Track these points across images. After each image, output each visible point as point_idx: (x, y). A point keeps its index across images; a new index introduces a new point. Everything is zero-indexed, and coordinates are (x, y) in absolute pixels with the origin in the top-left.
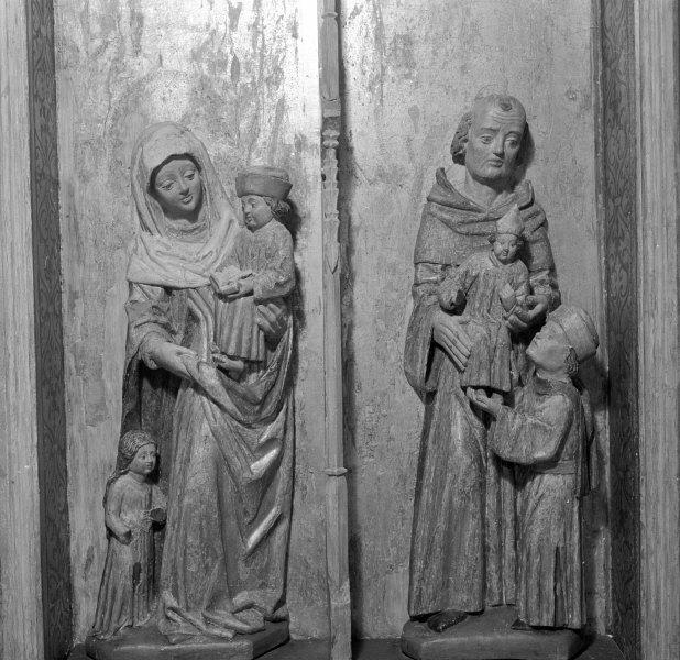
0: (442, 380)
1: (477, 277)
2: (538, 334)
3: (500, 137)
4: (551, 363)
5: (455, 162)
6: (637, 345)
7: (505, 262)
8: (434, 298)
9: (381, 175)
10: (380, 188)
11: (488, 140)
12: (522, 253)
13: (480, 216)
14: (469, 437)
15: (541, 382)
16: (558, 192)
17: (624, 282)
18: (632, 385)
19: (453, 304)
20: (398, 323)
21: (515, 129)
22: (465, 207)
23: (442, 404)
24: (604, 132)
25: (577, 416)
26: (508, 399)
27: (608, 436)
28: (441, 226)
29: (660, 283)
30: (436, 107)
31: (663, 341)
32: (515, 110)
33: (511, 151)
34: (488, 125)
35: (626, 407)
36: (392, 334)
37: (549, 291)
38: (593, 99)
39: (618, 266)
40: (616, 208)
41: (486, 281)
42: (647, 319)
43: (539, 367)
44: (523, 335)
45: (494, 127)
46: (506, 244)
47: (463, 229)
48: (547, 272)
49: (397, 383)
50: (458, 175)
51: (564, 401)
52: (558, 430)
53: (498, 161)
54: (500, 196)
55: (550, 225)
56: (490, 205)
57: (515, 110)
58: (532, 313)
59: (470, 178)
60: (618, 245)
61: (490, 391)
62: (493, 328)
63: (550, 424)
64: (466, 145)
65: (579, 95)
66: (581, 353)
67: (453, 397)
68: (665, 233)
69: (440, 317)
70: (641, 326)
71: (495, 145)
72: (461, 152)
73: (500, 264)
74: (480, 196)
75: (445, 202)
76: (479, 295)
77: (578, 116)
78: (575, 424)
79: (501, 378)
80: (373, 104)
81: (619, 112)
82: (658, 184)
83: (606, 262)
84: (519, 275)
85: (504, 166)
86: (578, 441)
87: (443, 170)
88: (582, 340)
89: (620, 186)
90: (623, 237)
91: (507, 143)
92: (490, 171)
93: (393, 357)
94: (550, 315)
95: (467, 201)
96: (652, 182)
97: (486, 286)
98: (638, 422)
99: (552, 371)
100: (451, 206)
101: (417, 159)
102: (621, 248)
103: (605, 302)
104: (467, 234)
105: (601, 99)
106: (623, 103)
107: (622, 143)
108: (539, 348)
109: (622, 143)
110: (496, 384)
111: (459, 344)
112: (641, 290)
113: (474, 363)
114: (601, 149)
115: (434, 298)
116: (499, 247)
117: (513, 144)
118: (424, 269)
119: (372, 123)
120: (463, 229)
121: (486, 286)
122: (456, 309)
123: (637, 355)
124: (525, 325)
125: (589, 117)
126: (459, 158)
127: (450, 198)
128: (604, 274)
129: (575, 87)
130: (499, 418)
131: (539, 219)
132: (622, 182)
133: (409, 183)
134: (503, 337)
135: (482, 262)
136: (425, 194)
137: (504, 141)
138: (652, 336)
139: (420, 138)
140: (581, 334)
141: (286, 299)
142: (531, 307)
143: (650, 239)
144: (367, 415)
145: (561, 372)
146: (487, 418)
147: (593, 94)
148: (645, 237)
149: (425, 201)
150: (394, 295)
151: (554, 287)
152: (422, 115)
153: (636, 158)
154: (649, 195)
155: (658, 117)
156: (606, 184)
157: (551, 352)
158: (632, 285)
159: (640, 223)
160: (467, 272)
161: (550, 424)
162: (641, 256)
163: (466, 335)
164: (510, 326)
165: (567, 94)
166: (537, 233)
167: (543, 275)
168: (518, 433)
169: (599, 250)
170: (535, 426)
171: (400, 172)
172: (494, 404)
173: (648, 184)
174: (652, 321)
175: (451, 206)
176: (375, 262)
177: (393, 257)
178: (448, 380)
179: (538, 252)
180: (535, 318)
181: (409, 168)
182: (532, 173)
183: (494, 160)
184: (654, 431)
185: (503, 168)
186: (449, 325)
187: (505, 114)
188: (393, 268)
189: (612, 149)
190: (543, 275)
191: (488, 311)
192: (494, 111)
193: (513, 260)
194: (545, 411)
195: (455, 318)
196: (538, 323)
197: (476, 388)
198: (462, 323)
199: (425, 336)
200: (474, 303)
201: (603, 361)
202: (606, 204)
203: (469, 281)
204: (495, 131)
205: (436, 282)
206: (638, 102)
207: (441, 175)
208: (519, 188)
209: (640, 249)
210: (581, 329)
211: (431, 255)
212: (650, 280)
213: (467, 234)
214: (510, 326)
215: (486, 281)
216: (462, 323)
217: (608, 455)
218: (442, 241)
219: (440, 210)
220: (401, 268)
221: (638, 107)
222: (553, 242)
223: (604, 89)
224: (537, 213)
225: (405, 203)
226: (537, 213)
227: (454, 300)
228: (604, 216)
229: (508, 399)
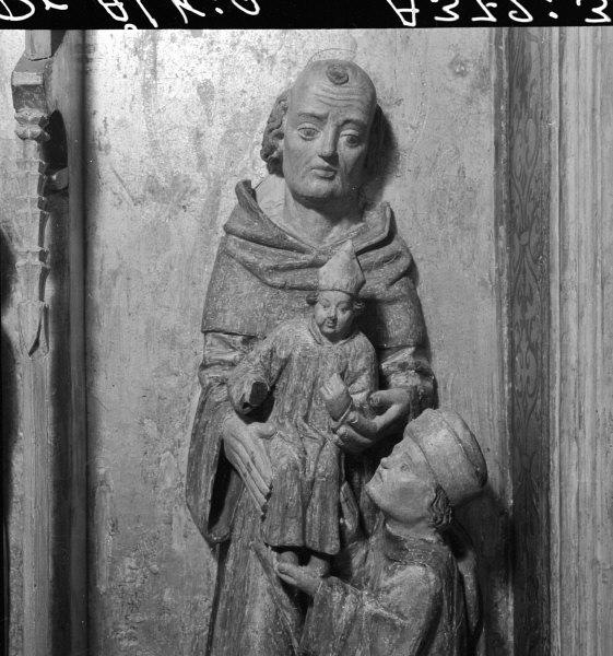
0: (238, 524)
1: (287, 361)
2: (384, 460)
3: (329, 129)
4: (405, 510)
5: (66, 166)
6: (548, 489)
7: (333, 338)
8: (223, 392)
9: (153, 189)
10: (150, 211)
11: (310, 135)
12: (365, 317)
13: (304, 258)
14: (276, 619)
15: (392, 539)
16: (434, 220)
17: (531, 372)
18: (542, 551)
19: (246, 405)
20: (177, 426)
21: (355, 115)
22: (280, 243)
23: (237, 563)
24: (509, 126)
25: (451, 603)
26: (338, 568)
27: (511, 608)
28: (243, 275)
29: (588, 383)
30: (241, 84)
31: (594, 484)
32: (354, 84)
33: (348, 153)
34: (310, 109)
35: (534, 583)
36: (169, 444)
37: (415, 381)
38: (493, 76)
39: (524, 346)
40: (523, 249)
41: (303, 368)
42: (565, 443)
43: (389, 516)
44: (361, 457)
45: (319, 112)
46: (332, 307)
47: (278, 280)
48: (411, 350)
49: (175, 520)
50: (273, 193)
51: (426, 577)
52: (415, 626)
53: (327, 169)
54: (336, 229)
55: (421, 275)
56: (320, 242)
57: (354, 84)
58: (379, 421)
59: (290, 197)
60: (525, 309)
61: (303, 555)
62: (312, 447)
63: (401, 615)
64: (281, 143)
65: (471, 68)
66: (454, 495)
67: (252, 553)
68: (599, 295)
69: (232, 421)
70: (555, 456)
71: (322, 143)
72: (275, 154)
73: (325, 340)
74: (304, 226)
75: (251, 234)
76: (290, 391)
77: (470, 101)
78: (445, 613)
79: (323, 533)
80: (141, 75)
81: (528, 90)
82: (589, 209)
83: (511, 334)
84: (359, 357)
85: (338, 178)
86: (451, 639)
87: (247, 183)
88: (458, 473)
89: (529, 213)
90: (530, 299)
91: (343, 140)
92: (317, 186)
93: (169, 480)
94: (412, 425)
95: (282, 235)
96: (577, 206)
97: (302, 376)
98: (549, 623)
99: (409, 523)
100: (257, 241)
101: (211, 166)
102: (528, 316)
103: (507, 397)
104: (282, 288)
105: (506, 75)
106: (532, 76)
107: (532, 138)
108: (389, 481)
109: (532, 138)
110: (313, 541)
111: (255, 471)
112: (556, 393)
113: (276, 506)
114: (504, 154)
115: (223, 392)
116: (322, 313)
117: (353, 141)
118: (215, 341)
119: (139, 107)
120: (278, 280)
121: (302, 376)
122: (258, 408)
123: (548, 506)
124: (366, 440)
125: (486, 104)
126: (275, 166)
127: (256, 229)
128: (506, 353)
129: (465, 55)
130: (316, 603)
131: (403, 263)
132: (531, 205)
133: (198, 202)
134: (324, 462)
135: (298, 334)
136: (223, 219)
137: (337, 135)
138: (574, 474)
139: (215, 132)
140: (453, 464)
141: (405, 274)
142: (381, 409)
143: (572, 308)
144: (128, 571)
145: (422, 524)
146: (301, 599)
147: (493, 66)
148: (563, 301)
149: (222, 233)
150: (173, 382)
151: (424, 373)
152: (218, 96)
153: (549, 165)
154: (572, 232)
155: (590, 92)
156: (511, 210)
157: (405, 492)
158: (542, 381)
159: (555, 277)
160: (272, 351)
161: (401, 615)
162: (556, 336)
163: (265, 455)
164: (341, 443)
165: (452, 64)
166: (396, 287)
167: (406, 355)
168: (349, 628)
169: (499, 316)
170: (376, 618)
171: (184, 186)
172: (309, 575)
173: (571, 209)
174: (574, 449)
175: (257, 241)
176: (142, 329)
177: (172, 320)
178: (245, 530)
179: (397, 321)
180: (387, 427)
181: (198, 179)
182: (394, 193)
183: (319, 168)
184: (578, 642)
185: (338, 180)
186: (246, 438)
187: (337, 89)
188: (171, 339)
189: (519, 152)
190: (406, 355)
191: (306, 418)
192: (321, 86)
193: (348, 332)
194: (393, 593)
195: (256, 426)
196: (393, 435)
197: (280, 549)
198: (267, 437)
199: (211, 451)
200: (283, 404)
201: (503, 492)
202: (510, 242)
203: (276, 367)
204: (321, 119)
205: (233, 364)
206: (555, 66)
207: (247, 192)
208: (373, 217)
209: (556, 322)
210: (454, 455)
211: (229, 320)
212: (572, 377)
213: (282, 288)
214: (341, 443)
215: (303, 368)
216: (267, 437)
217: (511, 639)
218: (245, 299)
219: (243, 247)
220: (185, 338)
221: (556, 75)
222: (426, 301)
223: (511, 58)
224: (398, 256)
225: (192, 235)
226: (398, 256)
227: (247, 399)
228: (507, 260)
229: (338, 568)
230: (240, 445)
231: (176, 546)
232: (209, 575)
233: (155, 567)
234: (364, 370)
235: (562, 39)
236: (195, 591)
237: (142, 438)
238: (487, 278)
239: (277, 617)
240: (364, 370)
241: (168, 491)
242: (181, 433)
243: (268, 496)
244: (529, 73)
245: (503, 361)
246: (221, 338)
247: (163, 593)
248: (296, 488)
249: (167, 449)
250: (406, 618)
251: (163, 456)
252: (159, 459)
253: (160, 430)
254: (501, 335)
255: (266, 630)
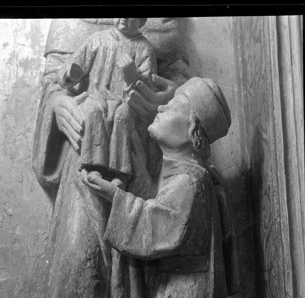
20: (28, 118)
36: (22, 130)
49: (25, 180)
61: (108, 174)
67: (73, 186)
146: (105, 202)
191: (108, 87)
227: (68, 74)
230: (65, 110)
231: (25, 198)
232: (47, 216)
233: (10, 211)
234: (147, 57)
235: (278, 24)
236: (37, 228)
237: (4, 126)
238: (227, 27)
239: (89, 225)
240: (147, 57)
241: (20, 161)
242: (30, 123)
243: (82, 133)
244: (263, 162)
245: (239, 77)
246: (56, 56)
247: (15, 229)
248: (100, 125)
249: (21, 133)
250: (177, 210)
251: (18, 138)
252: (15, 140)
253: (16, 121)
254: (237, 62)
255: (81, 232)
